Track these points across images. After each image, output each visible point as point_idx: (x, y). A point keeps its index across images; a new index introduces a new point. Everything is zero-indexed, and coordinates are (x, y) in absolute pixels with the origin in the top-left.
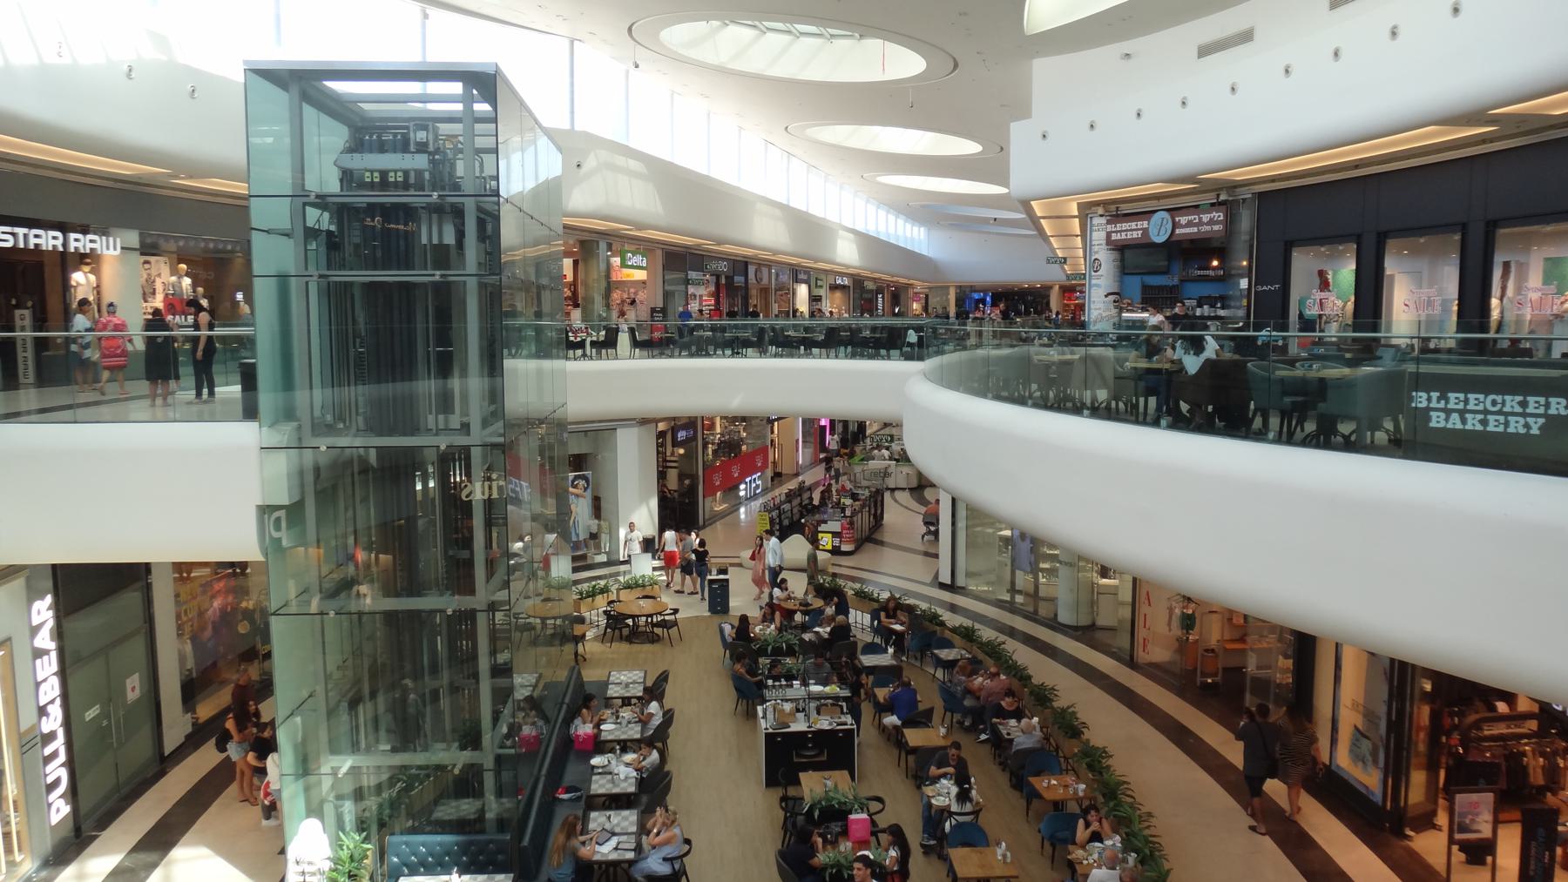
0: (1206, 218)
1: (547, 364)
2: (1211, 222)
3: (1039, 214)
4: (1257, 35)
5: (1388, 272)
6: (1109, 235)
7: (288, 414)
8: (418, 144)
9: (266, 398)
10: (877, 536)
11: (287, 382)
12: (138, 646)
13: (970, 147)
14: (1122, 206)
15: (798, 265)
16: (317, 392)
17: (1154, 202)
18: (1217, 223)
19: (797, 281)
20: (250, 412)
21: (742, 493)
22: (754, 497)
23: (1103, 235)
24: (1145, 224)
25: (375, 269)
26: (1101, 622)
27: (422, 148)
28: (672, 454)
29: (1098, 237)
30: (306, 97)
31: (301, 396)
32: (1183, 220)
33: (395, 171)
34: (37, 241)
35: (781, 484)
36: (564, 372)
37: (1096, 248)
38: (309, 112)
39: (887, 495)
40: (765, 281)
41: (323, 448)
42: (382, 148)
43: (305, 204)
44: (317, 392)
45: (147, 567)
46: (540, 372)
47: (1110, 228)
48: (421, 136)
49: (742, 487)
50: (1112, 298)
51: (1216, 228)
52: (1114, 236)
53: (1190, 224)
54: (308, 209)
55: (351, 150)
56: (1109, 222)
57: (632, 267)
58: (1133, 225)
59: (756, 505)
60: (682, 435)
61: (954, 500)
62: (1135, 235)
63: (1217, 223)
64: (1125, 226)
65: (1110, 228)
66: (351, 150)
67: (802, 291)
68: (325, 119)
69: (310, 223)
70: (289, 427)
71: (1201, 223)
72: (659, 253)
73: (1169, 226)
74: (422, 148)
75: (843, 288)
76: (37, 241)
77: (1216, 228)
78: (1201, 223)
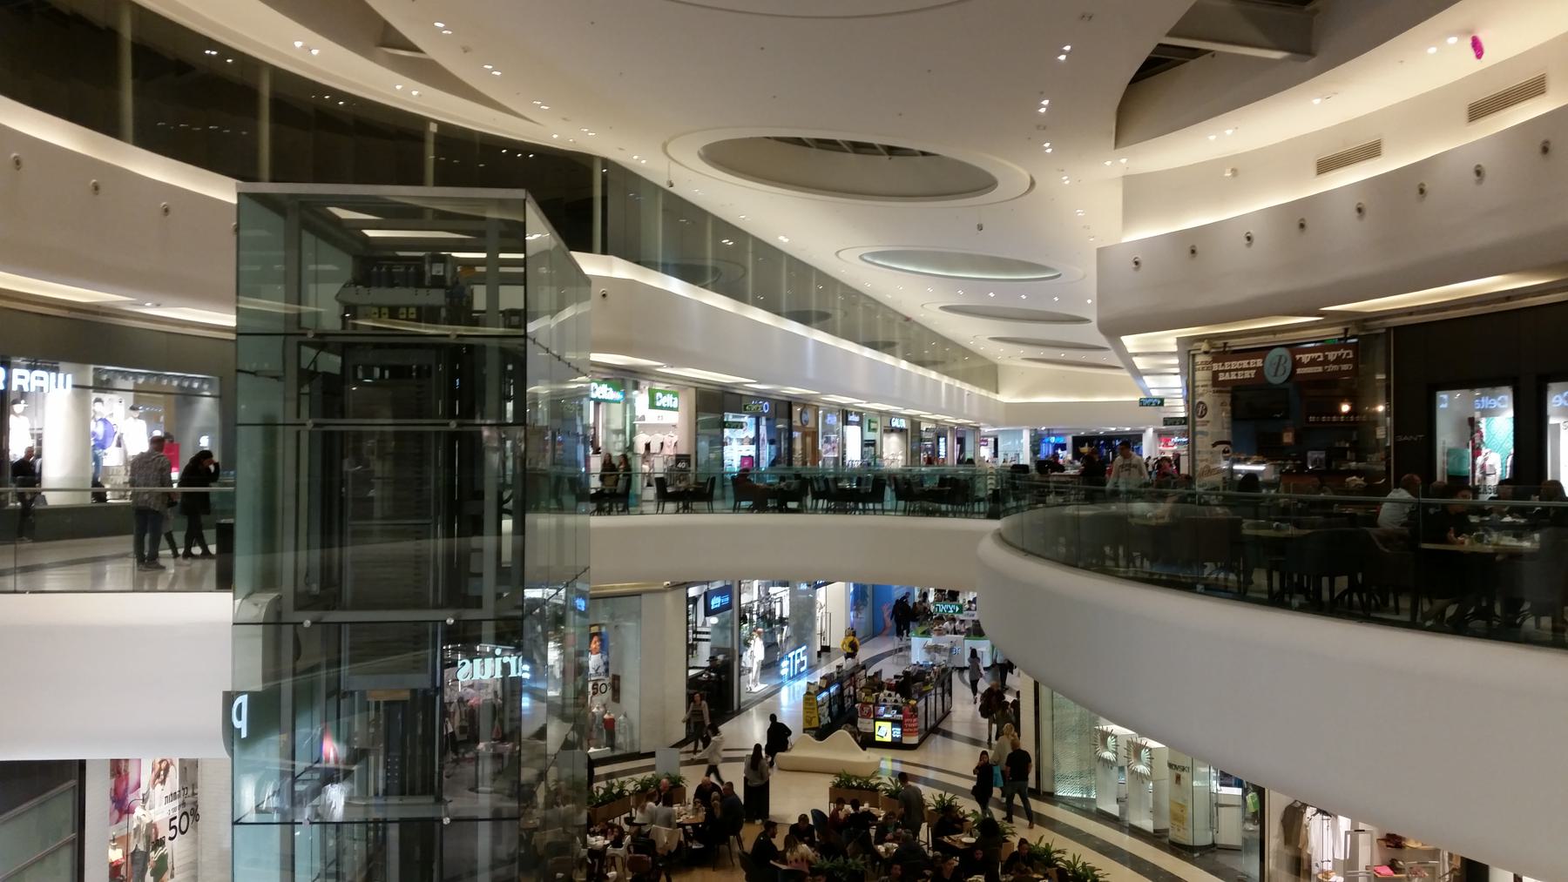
0: (1332, 356)
1: (569, 520)
2: (1339, 361)
3: (1130, 350)
4: (1384, 149)
5: (1552, 421)
6: (1215, 374)
7: (267, 580)
8: (434, 278)
9: (244, 562)
10: (943, 726)
11: (269, 541)
12: (66, 856)
13: (502, 269)
14: (1231, 342)
15: (850, 405)
16: (303, 554)
17: (1270, 338)
18: (1346, 361)
19: (846, 422)
20: (225, 581)
21: (784, 672)
22: (798, 676)
23: (1208, 374)
24: (1259, 362)
25: (342, 432)
26: (1223, 840)
27: (438, 282)
28: (704, 624)
29: (1202, 376)
30: (306, 225)
31: (287, 560)
32: (1305, 358)
33: (408, 308)
34: (21, 382)
35: (829, 660)
36: (587, 529)
37: (1200, 390)
38: (308, 239)
39: (955, 676)
40: (811, 425)
41: (307, 623)
42: (391, 281)
43: (300, 344)
44: (303, 554)
45: (77, 770)
46: (560, 527)
47: (1216, 367)
48: (438, 270)
49: (784, 664)
50: (1221, 447)
51: (1345, 367)
52: (1222, 377)
53: (1313, 363)
54: (304, 349)
55: (356, 282)
56: (1215, 360)
57: (661, 408)
58: (1245, 363)
59: (801, 685)
60: (716, 602)
61: (1036, 685)
62: (1247, 374)
63: (1346, 361)
64: (1235, 364)
65: (1216, 367)
66: (356, 282)
67: (853, 435)
68: (323, 245)
69: (305, 364)
70: (266, 598)
71: (1326, 362)
72: (693, 392)
73: (1289, 365)
74: (438, 282)
75: (900, 431)
76: (21, 382)
77: (1345, 367)
78: (1326, 362)
